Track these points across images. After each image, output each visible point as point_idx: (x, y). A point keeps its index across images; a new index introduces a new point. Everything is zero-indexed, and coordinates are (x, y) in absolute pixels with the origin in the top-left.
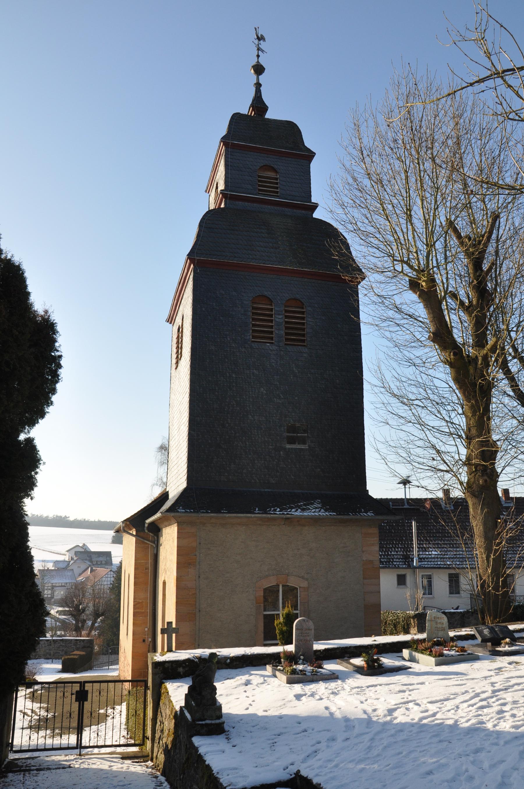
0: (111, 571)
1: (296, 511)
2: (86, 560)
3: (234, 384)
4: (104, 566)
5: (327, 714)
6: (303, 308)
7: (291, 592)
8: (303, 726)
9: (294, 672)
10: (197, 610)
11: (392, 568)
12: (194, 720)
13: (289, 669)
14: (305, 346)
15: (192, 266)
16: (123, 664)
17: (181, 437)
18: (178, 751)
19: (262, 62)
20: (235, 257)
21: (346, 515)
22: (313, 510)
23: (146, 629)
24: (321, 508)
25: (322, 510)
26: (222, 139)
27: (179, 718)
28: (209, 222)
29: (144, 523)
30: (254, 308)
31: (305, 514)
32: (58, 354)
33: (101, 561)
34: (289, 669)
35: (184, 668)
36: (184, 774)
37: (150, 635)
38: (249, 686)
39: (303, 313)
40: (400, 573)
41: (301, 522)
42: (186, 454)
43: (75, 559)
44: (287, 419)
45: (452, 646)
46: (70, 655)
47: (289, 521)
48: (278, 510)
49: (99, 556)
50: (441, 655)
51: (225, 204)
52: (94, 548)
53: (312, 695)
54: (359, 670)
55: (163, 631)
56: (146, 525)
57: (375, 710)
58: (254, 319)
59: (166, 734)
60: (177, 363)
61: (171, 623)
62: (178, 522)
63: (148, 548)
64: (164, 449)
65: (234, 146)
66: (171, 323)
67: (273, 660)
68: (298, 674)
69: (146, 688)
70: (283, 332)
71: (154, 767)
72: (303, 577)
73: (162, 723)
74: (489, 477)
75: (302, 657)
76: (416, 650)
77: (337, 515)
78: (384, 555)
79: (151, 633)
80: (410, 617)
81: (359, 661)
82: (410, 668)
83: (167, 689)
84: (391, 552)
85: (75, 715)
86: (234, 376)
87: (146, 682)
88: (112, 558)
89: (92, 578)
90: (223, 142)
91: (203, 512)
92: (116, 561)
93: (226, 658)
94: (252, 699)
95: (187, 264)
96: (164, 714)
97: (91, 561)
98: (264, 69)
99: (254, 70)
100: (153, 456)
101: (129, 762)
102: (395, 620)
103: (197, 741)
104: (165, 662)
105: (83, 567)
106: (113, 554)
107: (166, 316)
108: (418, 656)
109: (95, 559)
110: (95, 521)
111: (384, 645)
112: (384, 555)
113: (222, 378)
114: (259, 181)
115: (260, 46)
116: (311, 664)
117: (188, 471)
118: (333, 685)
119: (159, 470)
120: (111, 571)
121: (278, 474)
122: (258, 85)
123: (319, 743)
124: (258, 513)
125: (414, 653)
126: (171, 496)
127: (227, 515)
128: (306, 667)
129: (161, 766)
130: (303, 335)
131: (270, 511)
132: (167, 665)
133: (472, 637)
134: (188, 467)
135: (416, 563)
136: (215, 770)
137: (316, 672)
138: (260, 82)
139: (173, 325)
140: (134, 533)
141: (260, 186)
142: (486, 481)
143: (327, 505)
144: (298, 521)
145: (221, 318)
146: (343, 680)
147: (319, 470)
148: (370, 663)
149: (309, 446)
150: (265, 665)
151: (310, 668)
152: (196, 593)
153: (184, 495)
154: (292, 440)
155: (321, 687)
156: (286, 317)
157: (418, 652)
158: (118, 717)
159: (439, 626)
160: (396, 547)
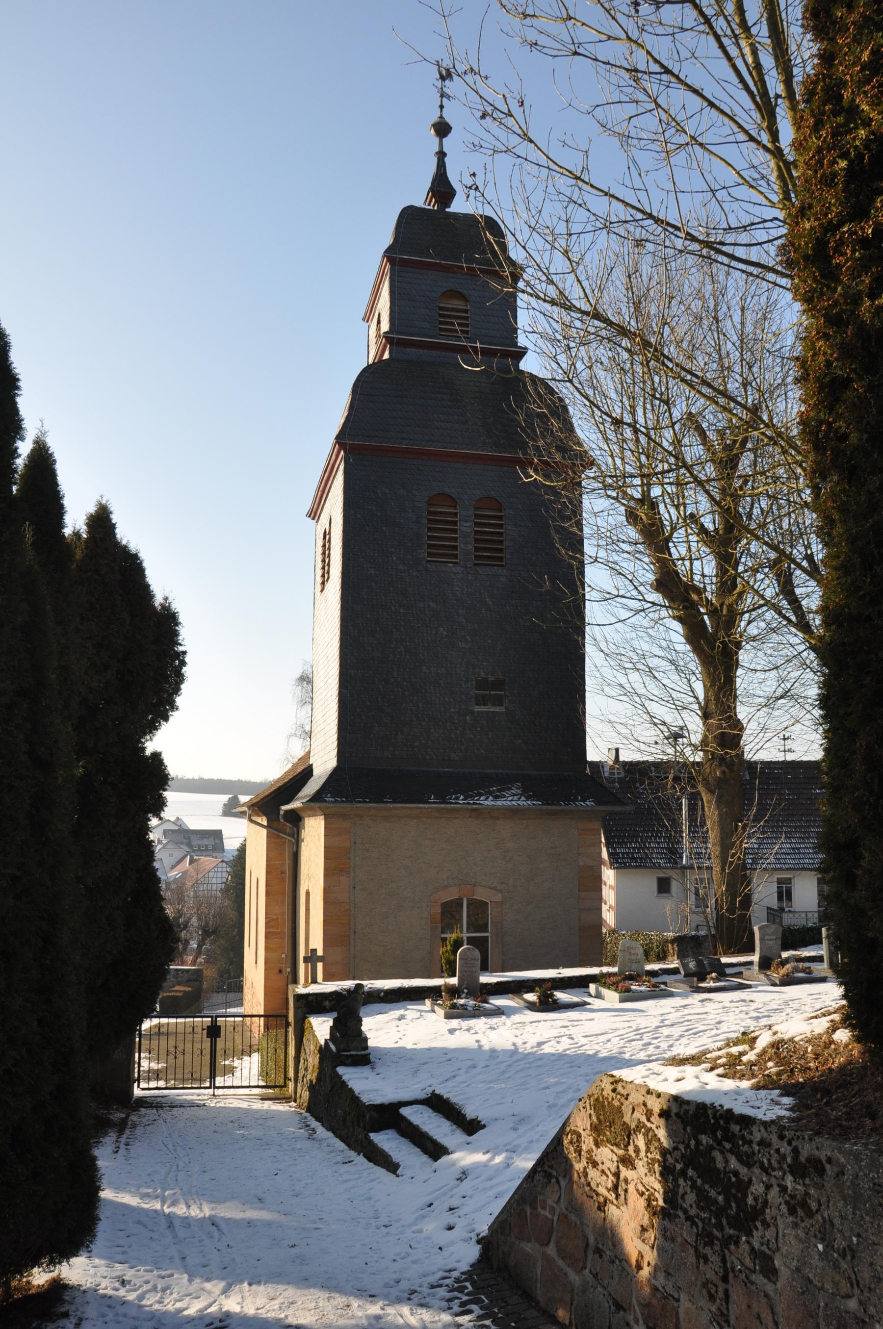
0: (222, 861)
1: (486, 800)
2: (182, 843)
3: (402, 623)
4: (209, 853)
5: (476, 1046)
6: (500, 511)
7: (478, 908)
8: (449, 1057)
9: (454, 1006)
10: (352, 932)
11: (650, 868)
12: (338, 1051)
13: (448, 1003)
14: (502, 566)
15: (342, 453)
16: (249, 1004)
17: (329, 694)
18: (322, 1084)
19: (448, 119)
20: (404, 439)
21: (555, 804)
22: (510, 798)
23: (284, 956)
24: (522, 795)
25: (523, 798)
26: (386, 252)
27: (324, 1051)
28: (369, 386)
29: (279, 810)
30: (430, 513)
31: (499, 803)
32: (181, 649)
33: (207, 846)
34: (448, 1003)
35: (330, 1001)
36: (329, 1102)
37: (289, 964)
38: (403, 1021)
39: (500, 518)
40: (662, 875)
41: (493, 814)
42: (336, 721)
43: (164, 842)
44: (477, 670)
45: (645, 981)
46: (170, 992)
47: (478, 813)
48: (462, 797)
49: (202, 838)
50: (628, 990)
51: (390, 353)
52: (193, 824)
53: (468, 1030)
54: (531, 1007)
55: (306, 960)
56: (282, 813)
57: (525, 1043)
58: (430, 529)
59: (310, 1071)
60: (323, 583)
61: (316, 950)
62: (325, 815)
63: (284, 843)
64: (306, 680)
65: (404, 263)
66: (313, 519)
67: (433, 993)
68: (458, 1009)
69: (288, 1024)
70: (471, 547)
71: (299, 1106)
72: (495, 888)
73: (306, 1060)
74: (728, 767)
75: (465, 991)
76: (605, 985)
77: (543, 804)
78: (638, 849)
79: (289, 961)
80: (667, 941)
81: (531, 997)
82: (589, 1004)
83: (311, 1024)
84: (649, 843)
85: (207, 1052)
86: (402, 611)
87: (287, 1017)
88: (224, 841)
89: (192, 872)
90: (387, 257)
91: (359, 802)
92: (231, 844)
93: (379, 991)
94: (403, 1033)
95: (336, 450)
96: (308, 1051)
97: (190, 845)
98: (451, 128)
99: (435, 131)
100: (290, 692)
101: (270, 1102)
102: (647, 945)
103: (340, 1070)
104: (308, 995)
105: (178, 854)
106: (225, 834)
107: (308, 506)
108: (604, 991)
109: (196, 842)
110: (193, 779)
111: (570, 978)
112: (638, 849)
113: (385, 614)
114: (441, 316)
115: (444, 89)
116: (475, 998)
117: (339, 745)
118: (494, 1021)
119: (299, 712)
120: (222, 861)
121: (463, 747)
122: (441, 155)
123: (460, 1069)
124: (434, 803)
125: (600, 988)
126: (316, 772)
127: (391, 806)
128: (470, 999)
129: (305, 1104)
130: (501, 551)
131: (450, 799)
132: (310, 998)
133: (675, 971)
134: (338, 739)
135: (687, 860)
136: (356, 1093)
137: (479, 1006)
138: (445, 150)
139: (317, 522)
140: (265, 823)
141: (441, 323)
142: (724, 772)
143: (530, 789)
144: (489, 813)
145: (384, 528)
146: (508, 1016)
147: (520, 741)
148: (542, 998)
149: (507, 708)
150: (424, 999)
151: (472, 1002)
152: (349, 910)
153: (334, 777)
154: (482, 701)
155: (480, 1023)
156: (477, 524)
157: (605, 987)
158: (248, 1069)
159: (633, 957)
160: (657, 835)
